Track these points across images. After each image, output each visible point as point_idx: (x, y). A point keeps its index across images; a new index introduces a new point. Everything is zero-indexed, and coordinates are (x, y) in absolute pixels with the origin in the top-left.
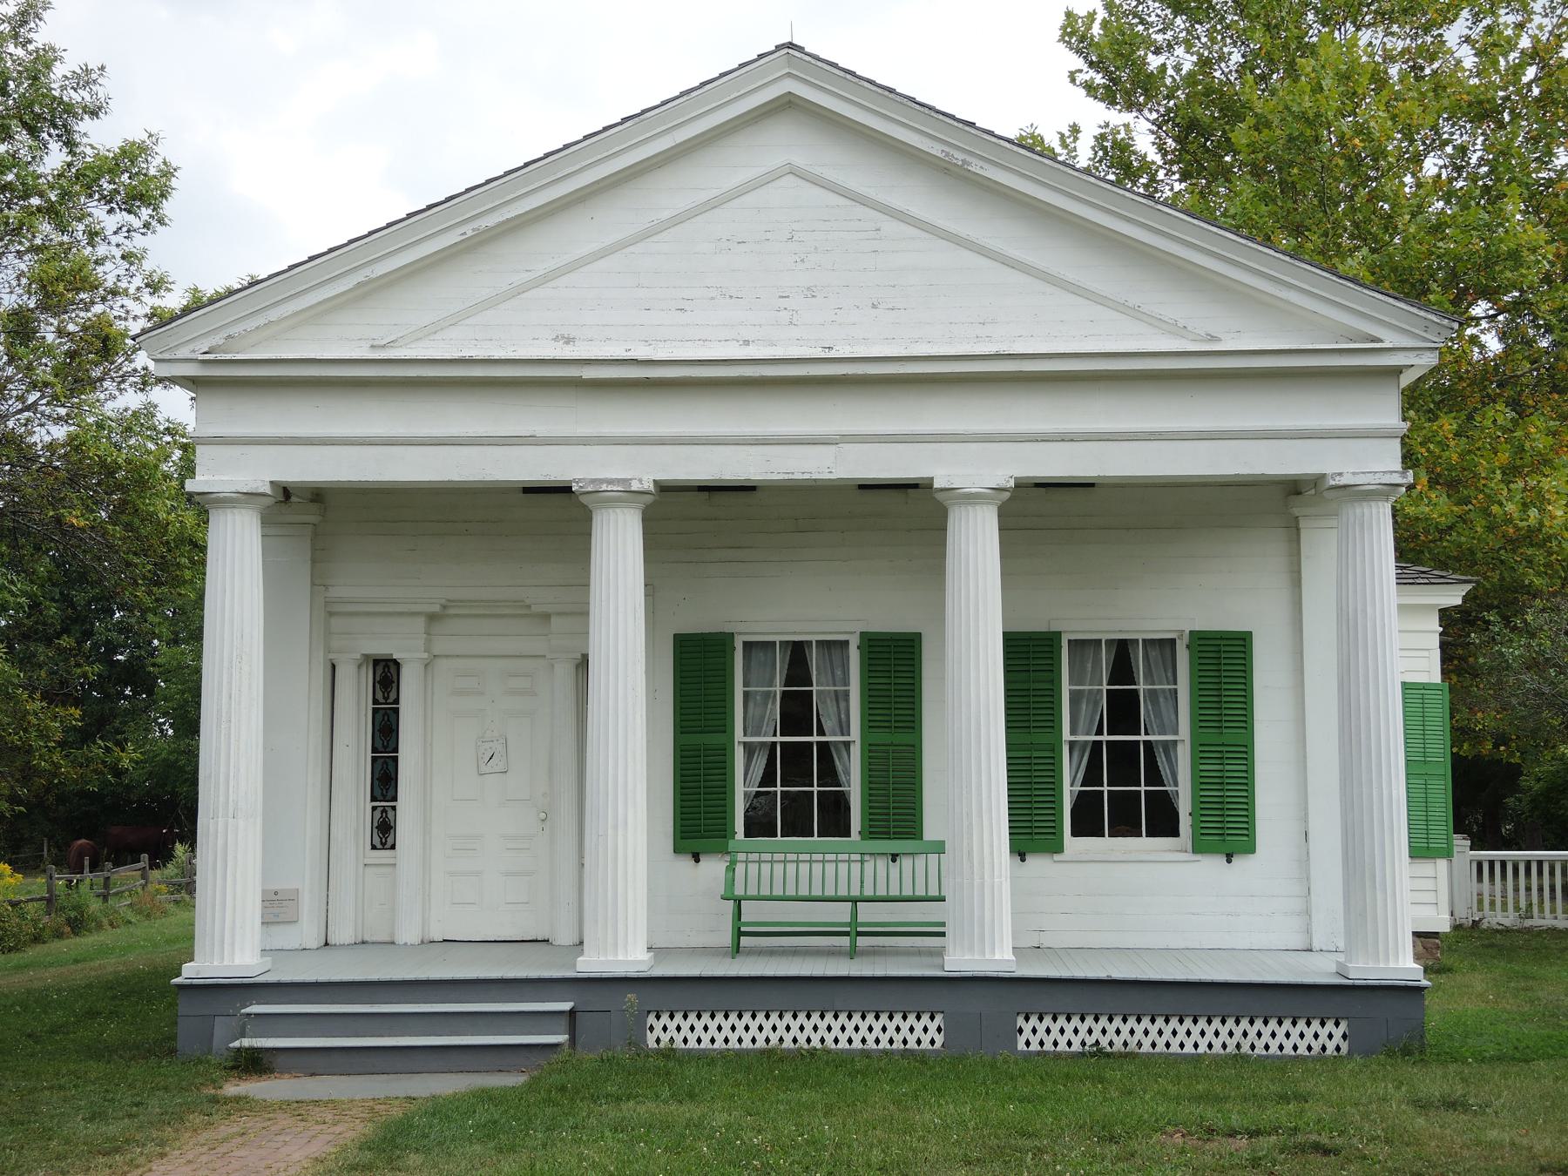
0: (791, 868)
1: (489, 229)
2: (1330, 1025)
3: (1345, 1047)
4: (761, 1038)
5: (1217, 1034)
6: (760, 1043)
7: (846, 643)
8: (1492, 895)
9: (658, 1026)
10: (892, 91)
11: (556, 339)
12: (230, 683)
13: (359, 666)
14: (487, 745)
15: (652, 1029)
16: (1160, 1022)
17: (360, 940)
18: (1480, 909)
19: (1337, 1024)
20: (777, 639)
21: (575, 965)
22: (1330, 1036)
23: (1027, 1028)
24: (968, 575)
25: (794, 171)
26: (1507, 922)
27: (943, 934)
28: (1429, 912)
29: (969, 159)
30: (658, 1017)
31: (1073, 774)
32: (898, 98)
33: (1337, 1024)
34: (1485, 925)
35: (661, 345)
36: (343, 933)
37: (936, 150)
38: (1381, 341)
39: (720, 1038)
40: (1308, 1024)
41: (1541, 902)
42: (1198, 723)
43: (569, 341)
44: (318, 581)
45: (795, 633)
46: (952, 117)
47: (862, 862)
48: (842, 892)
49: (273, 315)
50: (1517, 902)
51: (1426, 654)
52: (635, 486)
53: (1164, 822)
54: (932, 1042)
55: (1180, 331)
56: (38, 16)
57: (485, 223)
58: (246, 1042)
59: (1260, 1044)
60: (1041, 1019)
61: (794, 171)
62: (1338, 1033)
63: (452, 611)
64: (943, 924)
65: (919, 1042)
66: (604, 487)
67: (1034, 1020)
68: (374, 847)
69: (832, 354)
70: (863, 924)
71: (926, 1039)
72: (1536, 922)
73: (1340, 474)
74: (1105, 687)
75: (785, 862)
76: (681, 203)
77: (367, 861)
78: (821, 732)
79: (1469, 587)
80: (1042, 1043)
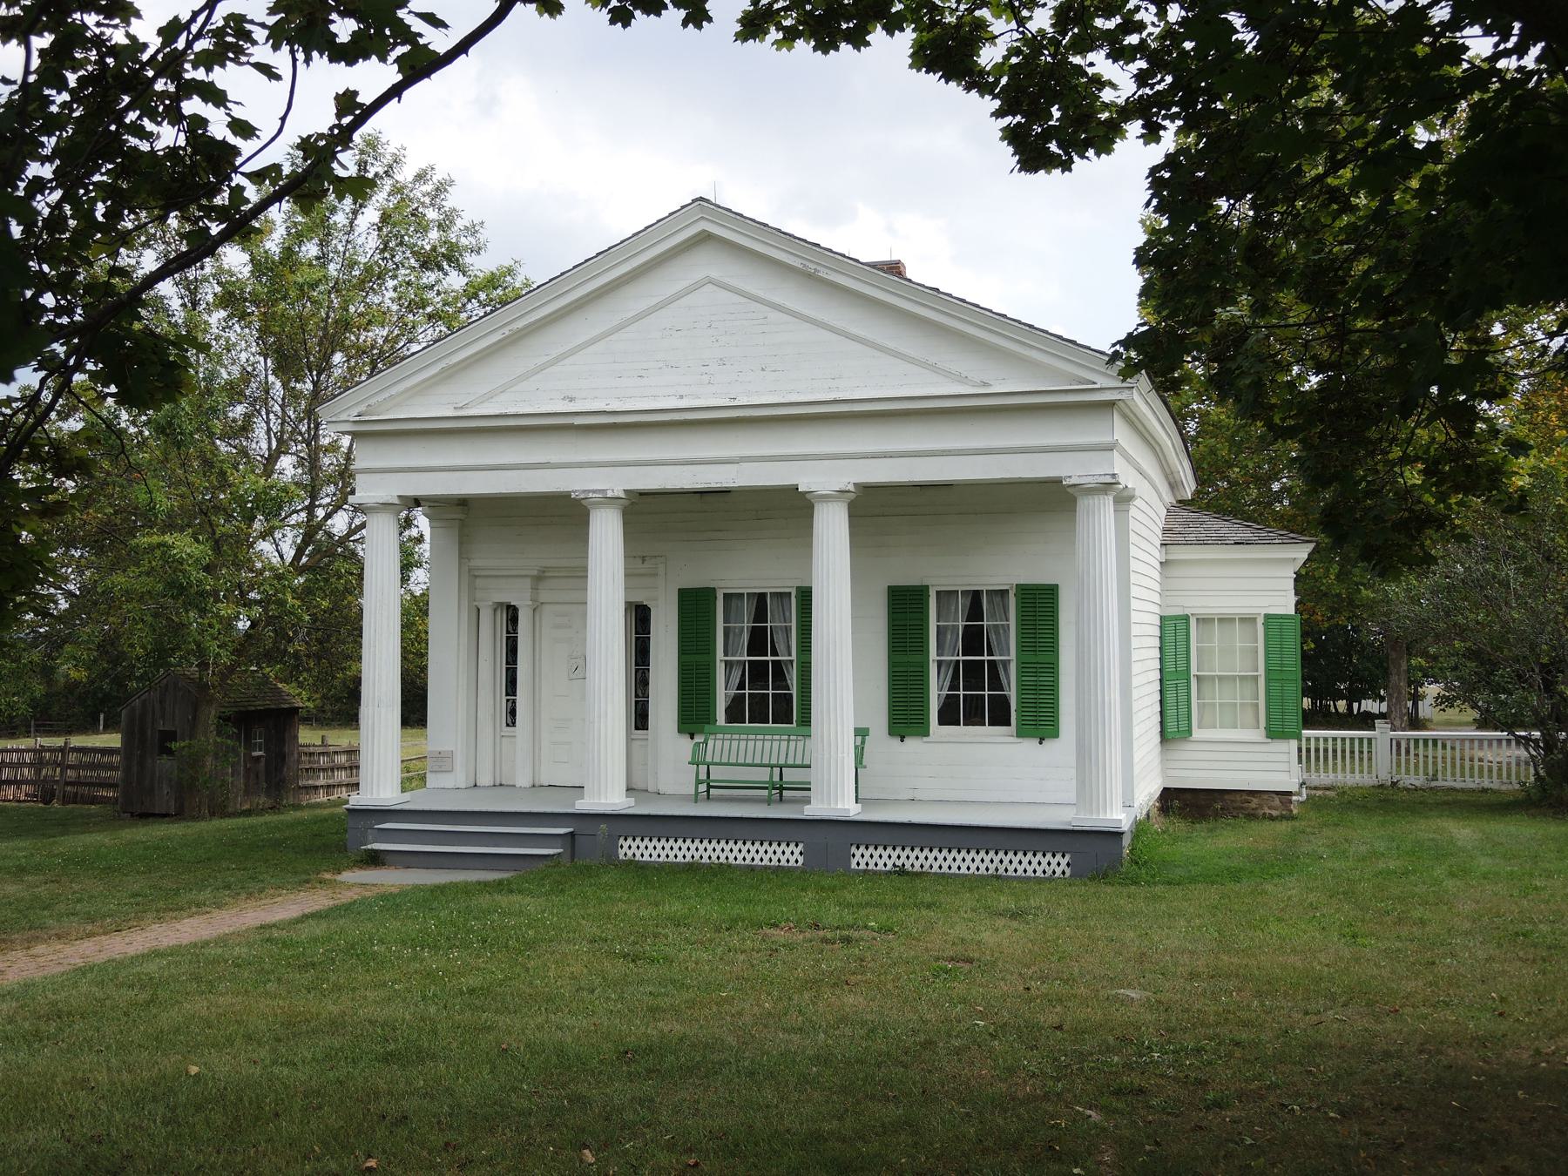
0: (735, 744)
1: (520, 330)
2: (1058, 857)
3: (1068, 872)
4: (689, 855)
5: (1030, 863)
6: (688, 859)
7: (790, 593)
8: (1453, 759)
9: (626, 845)
10: (766, 225)
11: (564, 399)
12: (375, 623)
13: (495, 610)
14: (574, 661)
15: (622, 847)
16: (945, 852)
17: (497, 783)
18: (1398, 772)
19: (1063, 856)
20: (745, 591)
21: (574, 805)
22: (1058, 864)
23: (857, 854)
24: (822, 552)
25: (712, 282)
26: (1418, 783)
27: (809, 789)
28: (1283, 777)
29: (818, 268)
30: (626, 840)
31: (941, 683)
32: (770, 230)
33: (1063, 856)
34: (1401, 784)
35: (628, 400)
36: (485, 779)
37: (796, 263)
38: (1094, 383)
39: (663, 855)
40: (1044, 855)
41: (1445, 768)
42: (1022, 648)
43: (571, 400)
44: (463, 556)
45: (755, 588)
46: (805, 241)
47: (789, 741)
48: (766, 761)
49: (394, 391)
50: (1426, 766)
51: (1283, 593)
52: (610, 494)
53: (1000, 717)
54: (797, 861)
55: (963, 380)
56: (446, 190)
57: (520, 324)
58: (369, 847)
59: (1011, 869)
60: (867, 848)
61: (712, 282)
62: (1064, 862)
63: (547, 574)
64: (810, 783)
65: (788, 861)
66: (591, 495)
67: (862, 849)
68: (508, 725)
69: (736, 403)
70: (786, 783)
71: (792, 860)
72: (1440, 783)
73: (1070, 477)
74: (985, 623)
75: (747, 740)
76: (644, 305)
77: (503, 734)
78: (774, 653)
79: (1312, 546)
80: (867, 864)
